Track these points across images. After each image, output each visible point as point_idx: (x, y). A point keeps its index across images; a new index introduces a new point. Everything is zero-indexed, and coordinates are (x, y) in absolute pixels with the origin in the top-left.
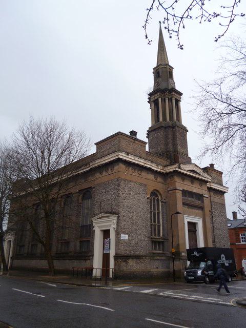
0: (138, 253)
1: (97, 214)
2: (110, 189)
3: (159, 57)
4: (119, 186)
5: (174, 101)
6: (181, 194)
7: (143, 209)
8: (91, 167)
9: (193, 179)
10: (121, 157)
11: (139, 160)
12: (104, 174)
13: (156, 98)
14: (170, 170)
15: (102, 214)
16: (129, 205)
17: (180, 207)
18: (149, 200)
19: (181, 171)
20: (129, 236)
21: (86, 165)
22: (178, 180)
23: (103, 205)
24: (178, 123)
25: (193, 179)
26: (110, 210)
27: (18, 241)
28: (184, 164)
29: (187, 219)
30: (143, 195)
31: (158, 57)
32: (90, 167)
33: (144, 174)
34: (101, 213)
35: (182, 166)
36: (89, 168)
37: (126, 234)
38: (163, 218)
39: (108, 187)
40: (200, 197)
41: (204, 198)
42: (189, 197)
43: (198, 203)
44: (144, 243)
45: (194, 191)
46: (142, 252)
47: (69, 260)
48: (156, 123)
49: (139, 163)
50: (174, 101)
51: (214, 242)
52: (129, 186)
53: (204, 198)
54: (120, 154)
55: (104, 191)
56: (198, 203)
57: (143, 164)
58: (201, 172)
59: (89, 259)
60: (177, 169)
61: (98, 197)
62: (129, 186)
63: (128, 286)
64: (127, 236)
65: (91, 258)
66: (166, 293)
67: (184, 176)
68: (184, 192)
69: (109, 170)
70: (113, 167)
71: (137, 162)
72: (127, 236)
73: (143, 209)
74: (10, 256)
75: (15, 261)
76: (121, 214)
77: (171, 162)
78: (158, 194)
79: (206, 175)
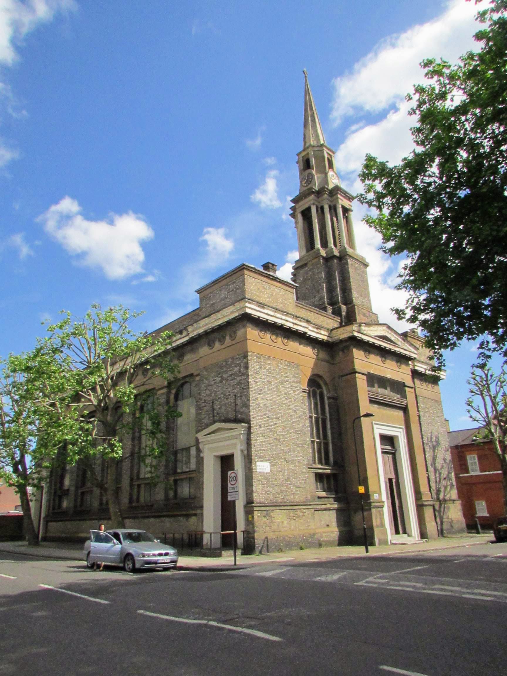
0: (290, 498)
1: (207, 426)
2: (231, 375)
3: (187, 316)
4: (247, 367)
5: (340, 211)
6: (365, 382)
7: (295, 412)
8: (191, 335)
9: (384, 353)
10: (248, 311)
11: (284, 317)
12: (217, 345)
13: (306, 206)
14: (342, 337)
15: (218, 425)
16: (269, 403)
17: (365, 406)
18: (306, 395)
19: (364, 337)
20: (272, 465)
21: (181, 332)
22: (357, 354)
23: (217, 407)
24: (349, 251)
25: (384, 353)
26: (231, 416)
27: (55, 485)
28: (368, 325)
29: (379, 430)
30: (294, 384)
31: (189, 313)
32: (188, 335)
33: (294, 345)
34: (214, 422)
35: (363, 328)
36: (187, 339)
37: (266, 461)
38: (332, 428)
39: (226, 372)
40: (399, 387)
41: (407, 389)
42: (379, 387)
43: (395, 397)
44: (302, 477)
45: (388, 376)
46: (299, 498)
47: (155, 517)
48: (308, 251)
49: (283, 322)
50: (340, 211)
51: (230, 495)
52: (268, 367)
53: (407, 389)
54: (247, 305)
55: (218, 379)
56: (395, 397)
57: (291, 325)
58: (399, 341)
59: (195, 515)
60: (356, 334)
61: (208, 392)
62: (268, 367)
63: (357, 586)
64: (268, 464)
65: (198, 511)
66: (371, 579)
67: (369, 347)
68: (374, 380)
69: (228, 338)
70: (235, 332)
71: (279, 322)
72: (268, 464)
73: (295, 412)
74: (43, 515)
75: (51, 524)
76: (253, 423)
77: (341, 323)
78: (321, 383)
79: (407, 346)
